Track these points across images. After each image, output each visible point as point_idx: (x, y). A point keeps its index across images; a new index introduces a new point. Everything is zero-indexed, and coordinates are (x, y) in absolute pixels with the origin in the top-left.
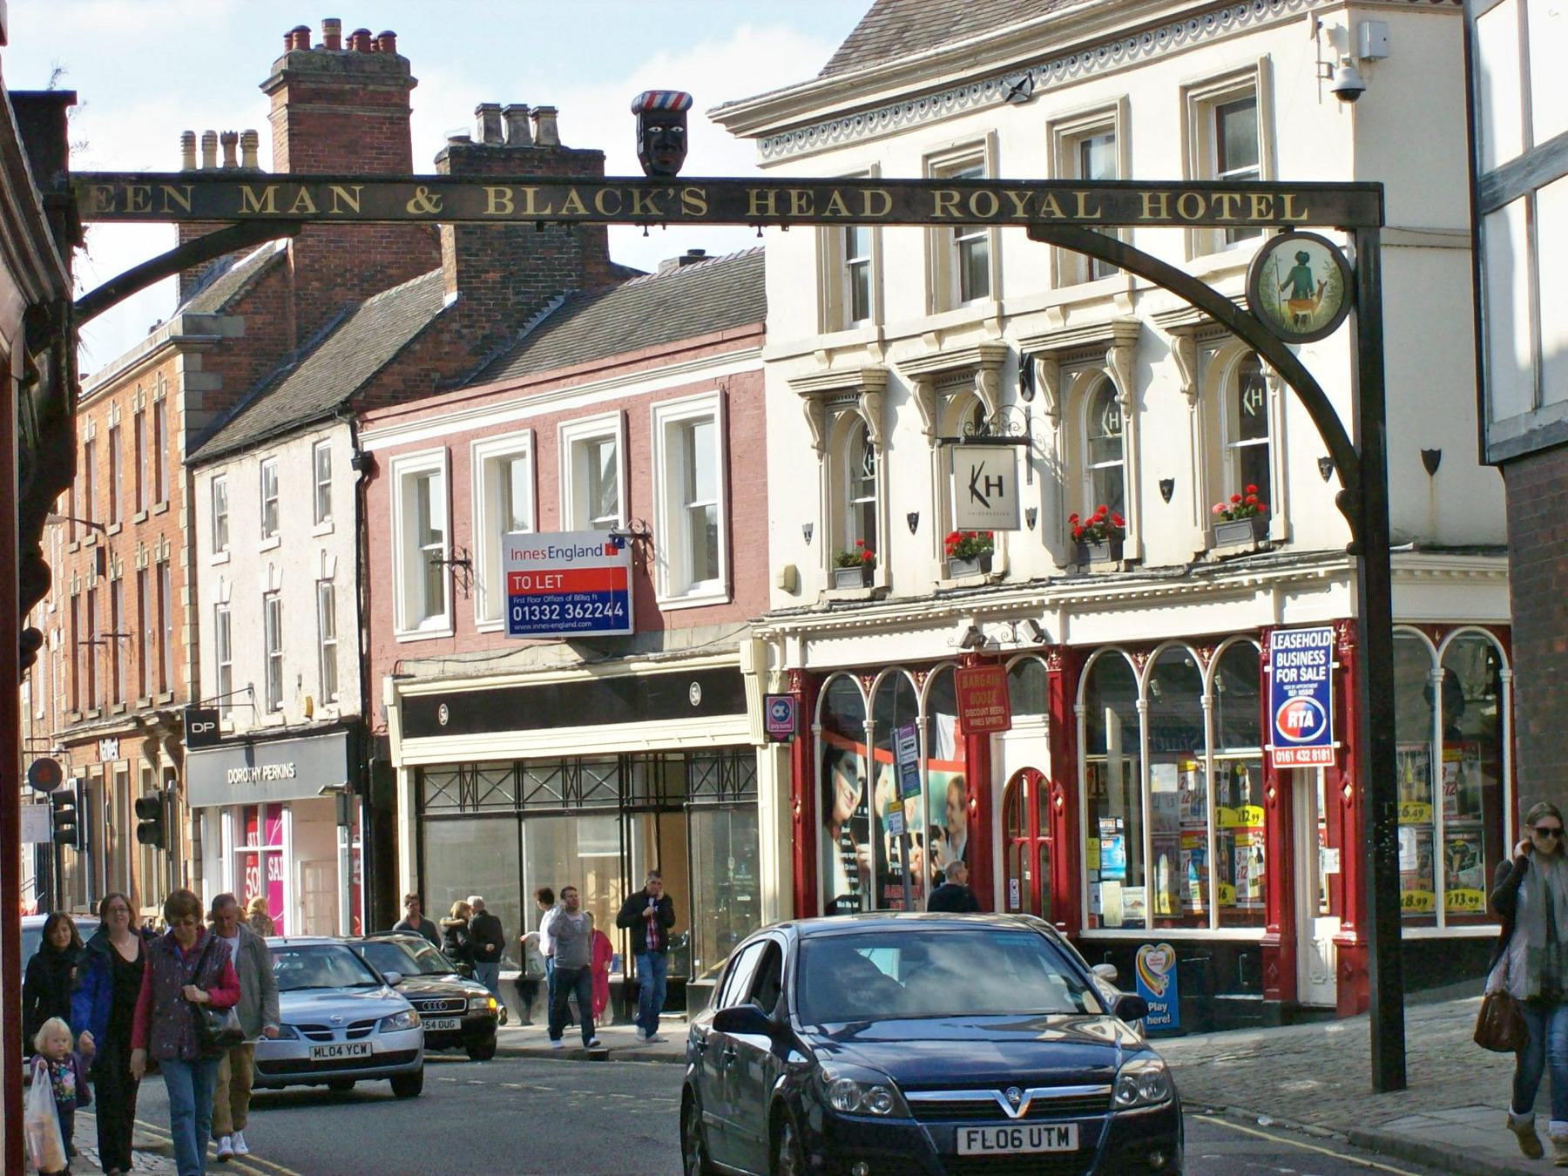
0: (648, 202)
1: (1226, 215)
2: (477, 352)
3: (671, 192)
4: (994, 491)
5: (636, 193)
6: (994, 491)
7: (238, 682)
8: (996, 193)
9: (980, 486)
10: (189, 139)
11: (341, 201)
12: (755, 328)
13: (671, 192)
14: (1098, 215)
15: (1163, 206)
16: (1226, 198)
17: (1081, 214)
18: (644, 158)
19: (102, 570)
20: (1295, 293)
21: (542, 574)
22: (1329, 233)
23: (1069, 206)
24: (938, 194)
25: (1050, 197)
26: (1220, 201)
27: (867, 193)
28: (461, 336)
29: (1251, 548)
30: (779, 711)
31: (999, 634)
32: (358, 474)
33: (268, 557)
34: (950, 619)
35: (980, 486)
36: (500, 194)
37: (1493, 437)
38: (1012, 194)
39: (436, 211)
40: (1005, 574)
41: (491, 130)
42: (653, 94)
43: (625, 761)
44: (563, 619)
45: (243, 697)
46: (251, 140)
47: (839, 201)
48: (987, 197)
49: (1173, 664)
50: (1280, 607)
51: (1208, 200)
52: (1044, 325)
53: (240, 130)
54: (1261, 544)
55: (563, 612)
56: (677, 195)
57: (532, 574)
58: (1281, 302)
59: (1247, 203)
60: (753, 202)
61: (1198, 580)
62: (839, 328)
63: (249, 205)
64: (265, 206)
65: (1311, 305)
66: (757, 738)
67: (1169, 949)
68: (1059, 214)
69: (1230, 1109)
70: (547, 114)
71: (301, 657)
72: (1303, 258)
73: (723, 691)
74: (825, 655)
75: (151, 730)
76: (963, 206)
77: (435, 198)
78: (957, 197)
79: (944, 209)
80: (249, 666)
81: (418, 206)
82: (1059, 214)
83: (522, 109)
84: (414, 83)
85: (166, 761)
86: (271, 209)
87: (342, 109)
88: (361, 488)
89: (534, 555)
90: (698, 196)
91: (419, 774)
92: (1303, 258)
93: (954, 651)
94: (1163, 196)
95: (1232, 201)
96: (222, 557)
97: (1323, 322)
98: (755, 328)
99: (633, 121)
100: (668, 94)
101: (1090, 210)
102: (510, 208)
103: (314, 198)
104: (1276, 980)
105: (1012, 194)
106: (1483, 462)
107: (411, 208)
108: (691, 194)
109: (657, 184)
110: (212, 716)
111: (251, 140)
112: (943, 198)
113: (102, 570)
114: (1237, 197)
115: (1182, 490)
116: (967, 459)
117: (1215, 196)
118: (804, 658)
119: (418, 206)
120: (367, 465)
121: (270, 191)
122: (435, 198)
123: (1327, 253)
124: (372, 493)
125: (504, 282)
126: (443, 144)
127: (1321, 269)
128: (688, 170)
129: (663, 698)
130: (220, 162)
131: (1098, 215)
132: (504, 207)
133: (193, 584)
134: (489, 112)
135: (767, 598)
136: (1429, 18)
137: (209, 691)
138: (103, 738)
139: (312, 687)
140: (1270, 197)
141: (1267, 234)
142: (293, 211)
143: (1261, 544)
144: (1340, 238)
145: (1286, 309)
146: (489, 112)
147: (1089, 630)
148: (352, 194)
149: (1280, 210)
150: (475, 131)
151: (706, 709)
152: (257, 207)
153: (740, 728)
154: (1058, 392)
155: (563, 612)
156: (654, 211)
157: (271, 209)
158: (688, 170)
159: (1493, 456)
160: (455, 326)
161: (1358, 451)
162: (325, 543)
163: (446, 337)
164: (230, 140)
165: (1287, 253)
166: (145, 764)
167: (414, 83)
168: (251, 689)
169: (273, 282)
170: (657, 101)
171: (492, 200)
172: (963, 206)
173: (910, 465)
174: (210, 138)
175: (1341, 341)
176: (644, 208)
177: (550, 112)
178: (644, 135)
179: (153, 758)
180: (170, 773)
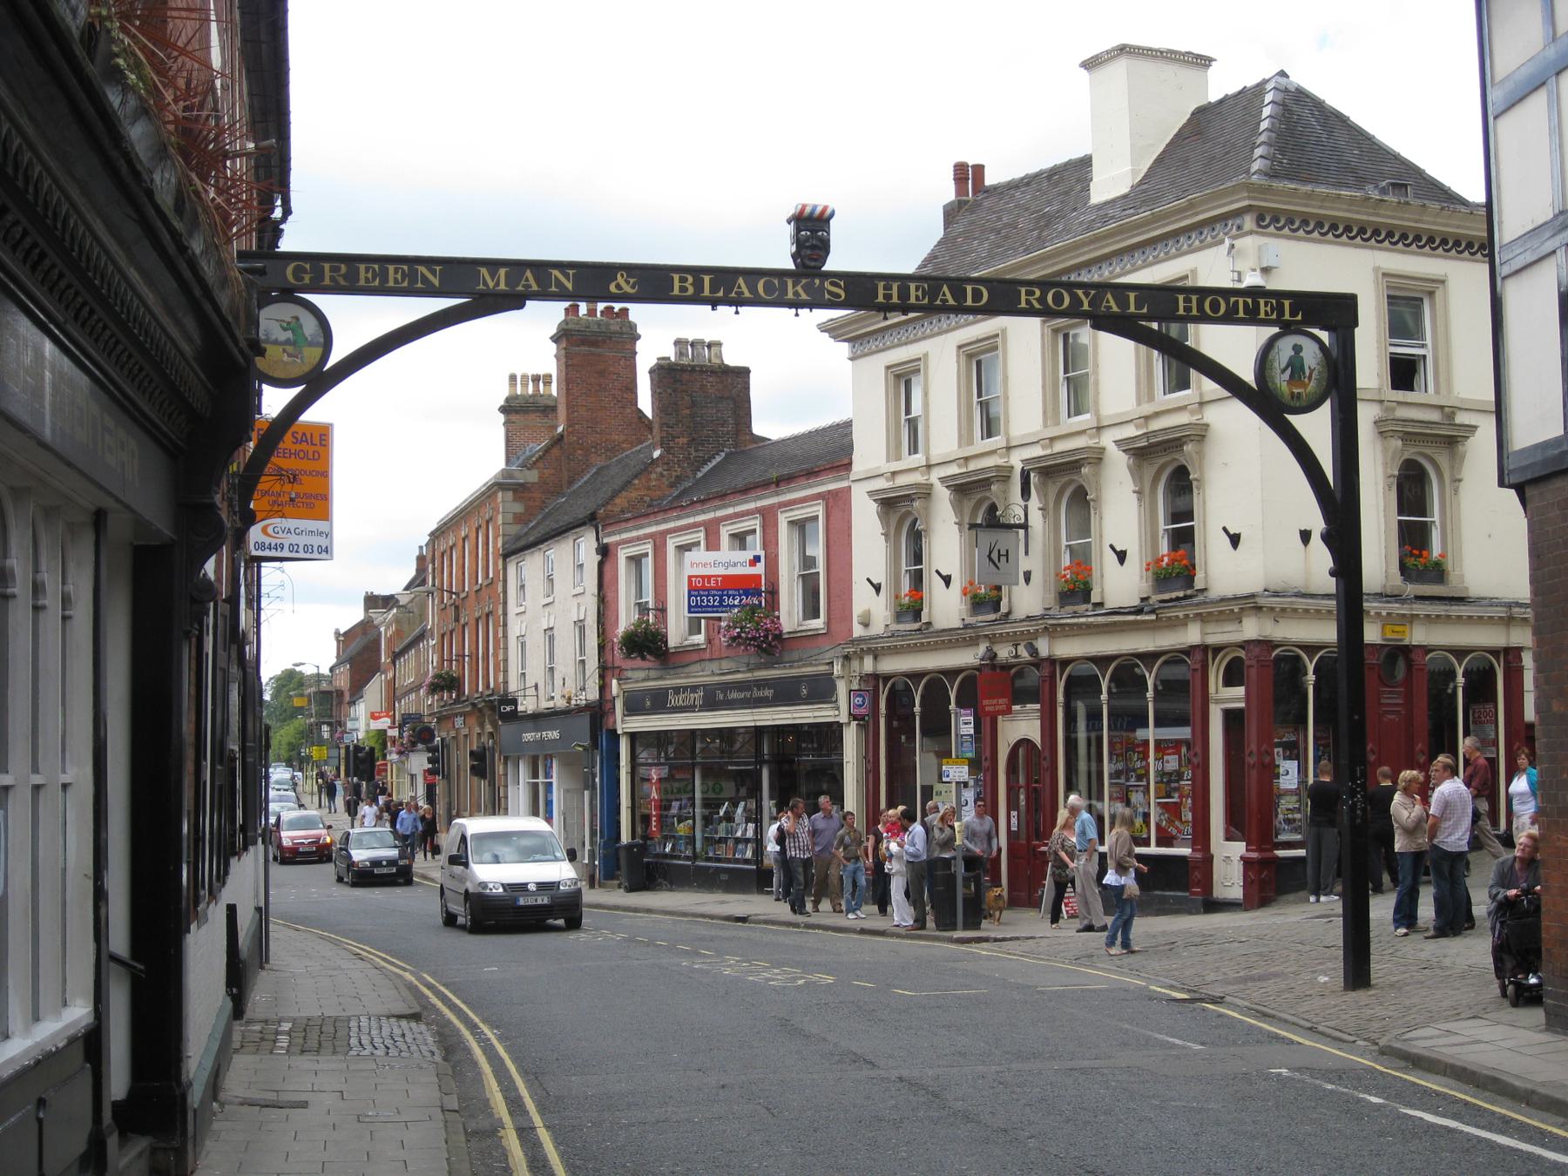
0: (799, 288)
1: (1241, 314)
2: (672, 485)
3: (817, 281)
4: (1003, 559)
5: (790, 283)
6: (1003, 559)
7: (530, 682)
9: (995, 556)
10: (513, 378)
11: (424, 277)
13: (817, 281)
17: (1132, 309)
18: (794, 256)
19: (457, 620)
20: (1292, 376)
21: (709, 577)
22: (1316, 331)
23: (1123, 303)
25: (1109, 296)
26: (1236, 303)
27: (969, 289)
28: (662, 475)
29: (1181, 594)
30: (859, 700)
31: (1004, 653)
32: (599, 558)
33: (548, 609)
34: (973, 642)
35: (995, 556)
37: (1511, 465)
38: (1080, 292)
39: (632, 291)
40: (1009, 613)
41: (681, 354)
42: (804, 206)
43: (759, 731)
44: (721, 605)
45: (532, 691)
46: (548, 382)
49: (1127, 672)
50: (1204, 634)
51: (1227, 303)
52: (1037, 451)
53: (541, 373)
54: (1189, 592)
55: (721, 601)
56: (822, 283)
57: (703, 577)
58: (1281, 381)
59: (1256, 305)
60: (881, 292)
61: (1141, 614)
62: (899, 458)
63: (485, 283)
64: (498, 284)
65: (1305, 386)
66: (843, 719)
68: (1115, 309)
69: (1228, 999)
70: (714, 345)
71: (566, 665)
72: (1297, 349)
73: (821, 690)
74: (890, 665)
75: (480, 710)
76: (1042, 300)
78: (1038, 293)
79: (1028, 302)
80: (536, 673)
81: (618, 286)
82: (1115, 309)
83: (702, 342)
84: (639, 337)
85: (489, 728)
86: (502, 286)
87: (599, 350)
88: (601, 565)
89: (705, 565)
90: (838, 286)
91: (633, 736)
92: (1297, 349)
93: (976, 662)
94: (1194, 298)
95: (1245, 303)
96: (522, 609)
97: (1304, 404)
99: (789, 229)
100: (815, 207)
101: (1138, 306)
103: (537, 280)
104: (1198, 884)
105: (1080, 292)
106: (1501, 484)
107: (612, 288)
108: (833, 284)
109: (806, 276)
110: (514, 702)
111: (547, 379)
113: (457, 620)
116: (987, 538)
118: (875, 666)
119: (618, 286)
120: (605, 552)
121: (502, 272)
123: (1315, 347)
124: (607, 567)
125: (689, 444)
126: (654, 362)
127: (1311, 356)
128: (831, 265)
129: (786, 693)
130: (530, 391)
132: (686, 290)
133: (505, 625)
134: (678, 343)
135: (851, 630)
137: (512, 687)
138: (456, 715)
139: (570, 684)
141: (1276, 330)
142: (520, 288)
143: (1189, 592)
144: (1324, 336)
145: (1285, 387)
146: (678, 343)
147: (1068, 648)
149: (1281, 313)
150: (670, 353)
151: (809, 700)
152: (491, 285)
153: (836, 711)
154: (1043, 495)
155: (721, 601)
156: (804, 296)
157: (502, 286)
158: (831, 265)
159: (1514, 479)
160: (659, 470)
161: (1338, 496)
162: (580, 600)
163: (653, 476)
164: (536, 379)
165: (1285, 349)
166: (478, 730)
167: (639, 337)
168: (536, 687)
169: (555, 451)
170: (808, 210)
172: (1042, 300)
173: (947, 545)
174: (524, 377)
175: (1325, 412)
176: (796, 294)
177: (719, 344)
178: (799, 242)
179: (482, 726)
180: (491, 734)
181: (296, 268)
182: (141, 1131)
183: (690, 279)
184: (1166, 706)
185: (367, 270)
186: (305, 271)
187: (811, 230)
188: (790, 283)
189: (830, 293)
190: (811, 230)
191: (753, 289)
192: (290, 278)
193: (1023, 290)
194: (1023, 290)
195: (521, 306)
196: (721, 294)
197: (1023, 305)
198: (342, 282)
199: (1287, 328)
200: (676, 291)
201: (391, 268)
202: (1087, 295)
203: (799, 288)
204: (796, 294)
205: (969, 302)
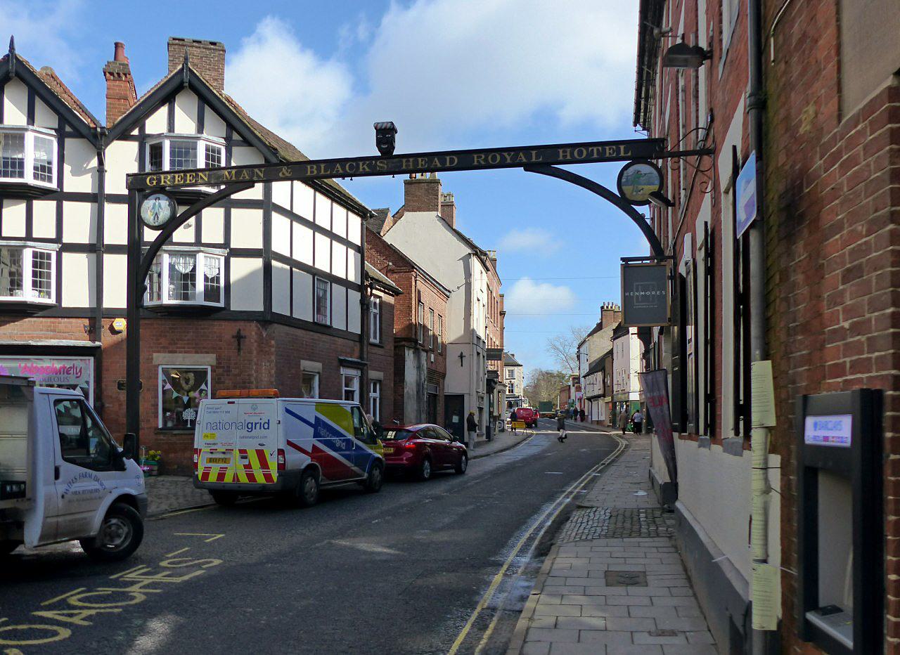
0: (365, 166)
8: (347, 172)
11: (201, 178)
12: (49, 520)
13: (374, 162)
14: (629, 154)
15: (568, 154)
16: (595, 149)
24: (309, 167)
36: (312, 168)
38: (506, 154)
47: (437, 161)
48: (582, 151)
51: (587, 150)
56: (376, 163)
67: (663, 337)
76: (486, 160)
77: (289, 170)
78: (483, 157)
81: (283, 174)
95: (598, 150)
98: (49, 520)
102: (315, 172)
108: (381, 162)
112: (478, 157)
114: (600, 148)
115: (476, 299)
117: (590, 149)
119: (283, 174)
122: (289, 170)
131: (629, 154)
136: (225, 71)
140: (614, 147)
142: (241, 178)
148: (261, 171)
156: (367, 170)
158: (395, 153)
171: (561, 154)
172: (486, 160)
181: (492, 156)
182: (215, 498)
183: (315, 167)
184: (848, 373)
185: (610, 149)
186: (154, 180)
187: (386, 135)
188: (361, 163)
189: (384, 163)
190: (386, 135)
191: (343, 168)
192: (148, 183)
193: (475, 156)
194: (475, 156)
195: (253, 186)
196: (329, 172)
197: (476, 163)
198: (483, 163)
199: (636, 160)
200: (561, 158)
201: (420, 159)
202: (509, 155)
203: (365, 166)
204: (364, 169)
205: (448, 165)
